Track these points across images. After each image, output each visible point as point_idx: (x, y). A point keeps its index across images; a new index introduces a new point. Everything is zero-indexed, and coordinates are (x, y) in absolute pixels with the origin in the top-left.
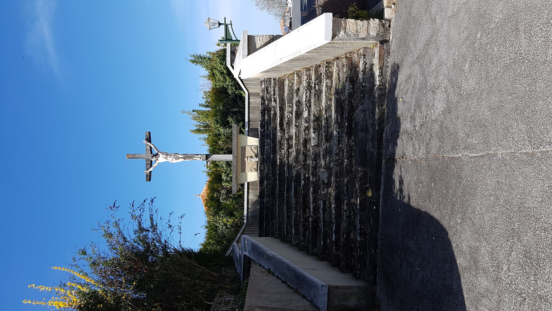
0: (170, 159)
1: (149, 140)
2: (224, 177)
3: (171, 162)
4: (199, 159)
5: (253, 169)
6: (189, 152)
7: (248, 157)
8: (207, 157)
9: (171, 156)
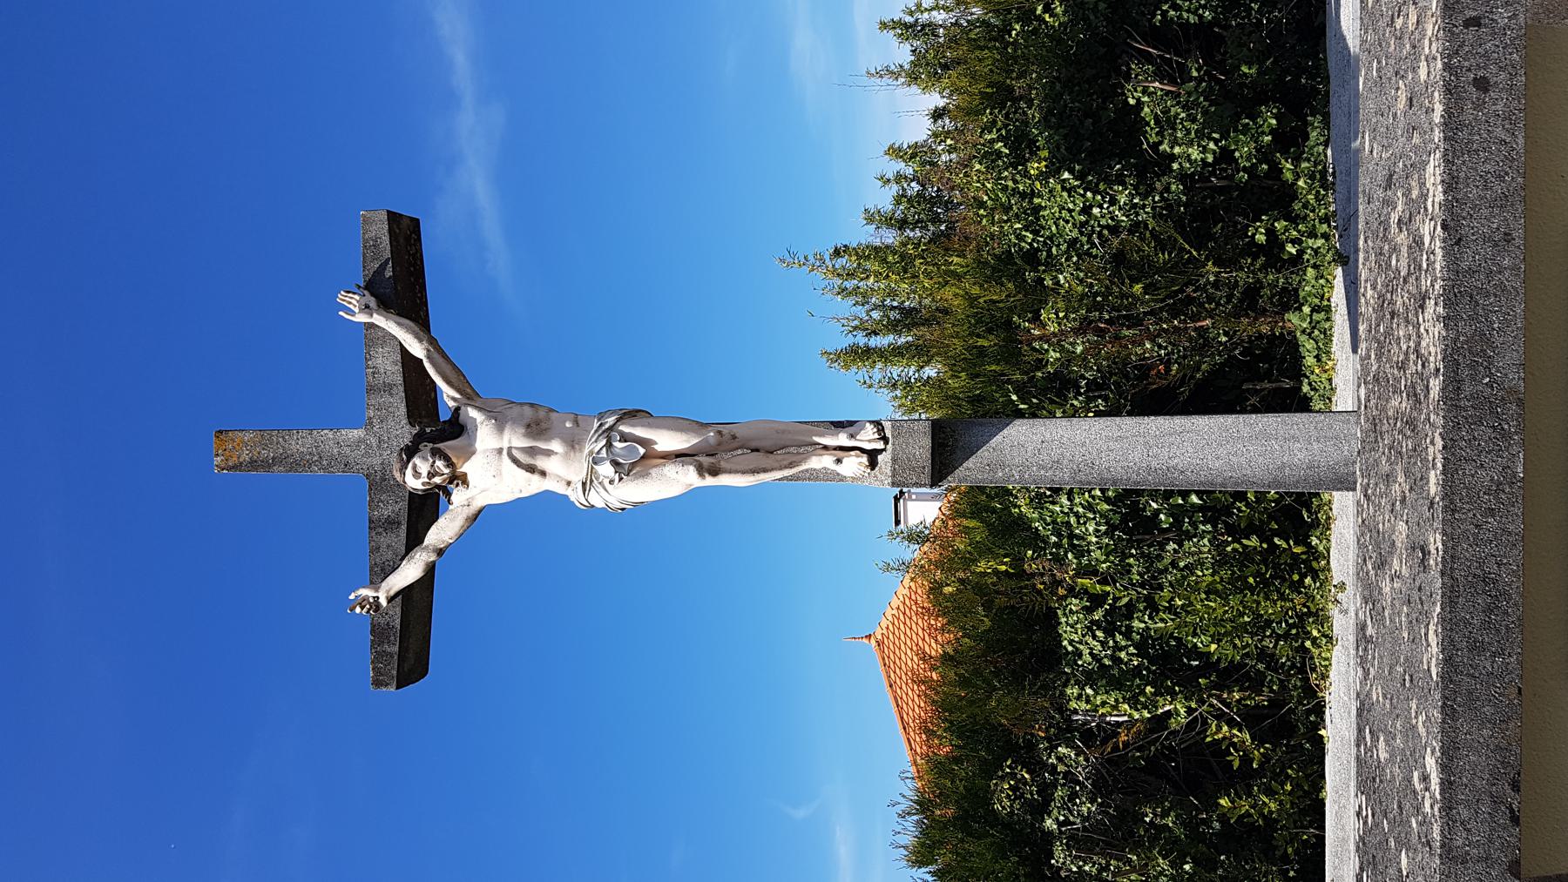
0: (563, 471)
1: (402, 285)
2: (1074, 630)
3: (576, 495)
4: (853, 465)
6: (752, 410)
9: (573, 444)
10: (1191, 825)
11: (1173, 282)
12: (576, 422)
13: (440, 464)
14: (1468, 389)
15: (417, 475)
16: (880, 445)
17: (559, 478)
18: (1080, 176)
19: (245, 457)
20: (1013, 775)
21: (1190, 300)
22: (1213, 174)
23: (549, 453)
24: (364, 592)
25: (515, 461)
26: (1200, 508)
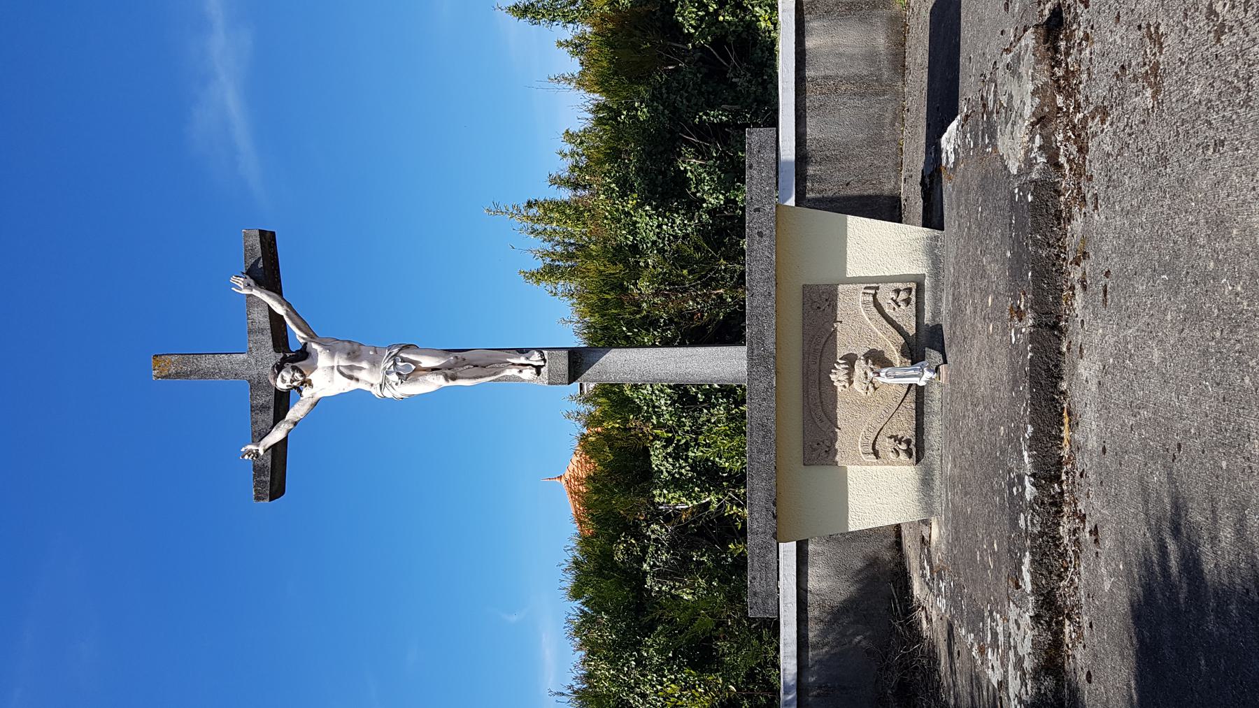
0: (369, 379)
1: (267, 274)
2: (658, 459)
3: (376, 391)
4: (528, 374)
5: (886, 445)
6: (480, 340)
7: (850, 360)
8: (577, 362)
9: (374, 363)
10: (717, 561)
11: (703, 269)
12: (376, 352)
13: (297, 375)
14: (756, 352)
15: (284, 381)
16: (542, 363)
17: (367, 382)
18: (655, 208)
19: (173, 370)
20: (625, 542)
21: (712, 279)
22: (725, 209)
23: (361, 369)
24: (253, 447)
25: (342, 373)
26: (719, 390)
